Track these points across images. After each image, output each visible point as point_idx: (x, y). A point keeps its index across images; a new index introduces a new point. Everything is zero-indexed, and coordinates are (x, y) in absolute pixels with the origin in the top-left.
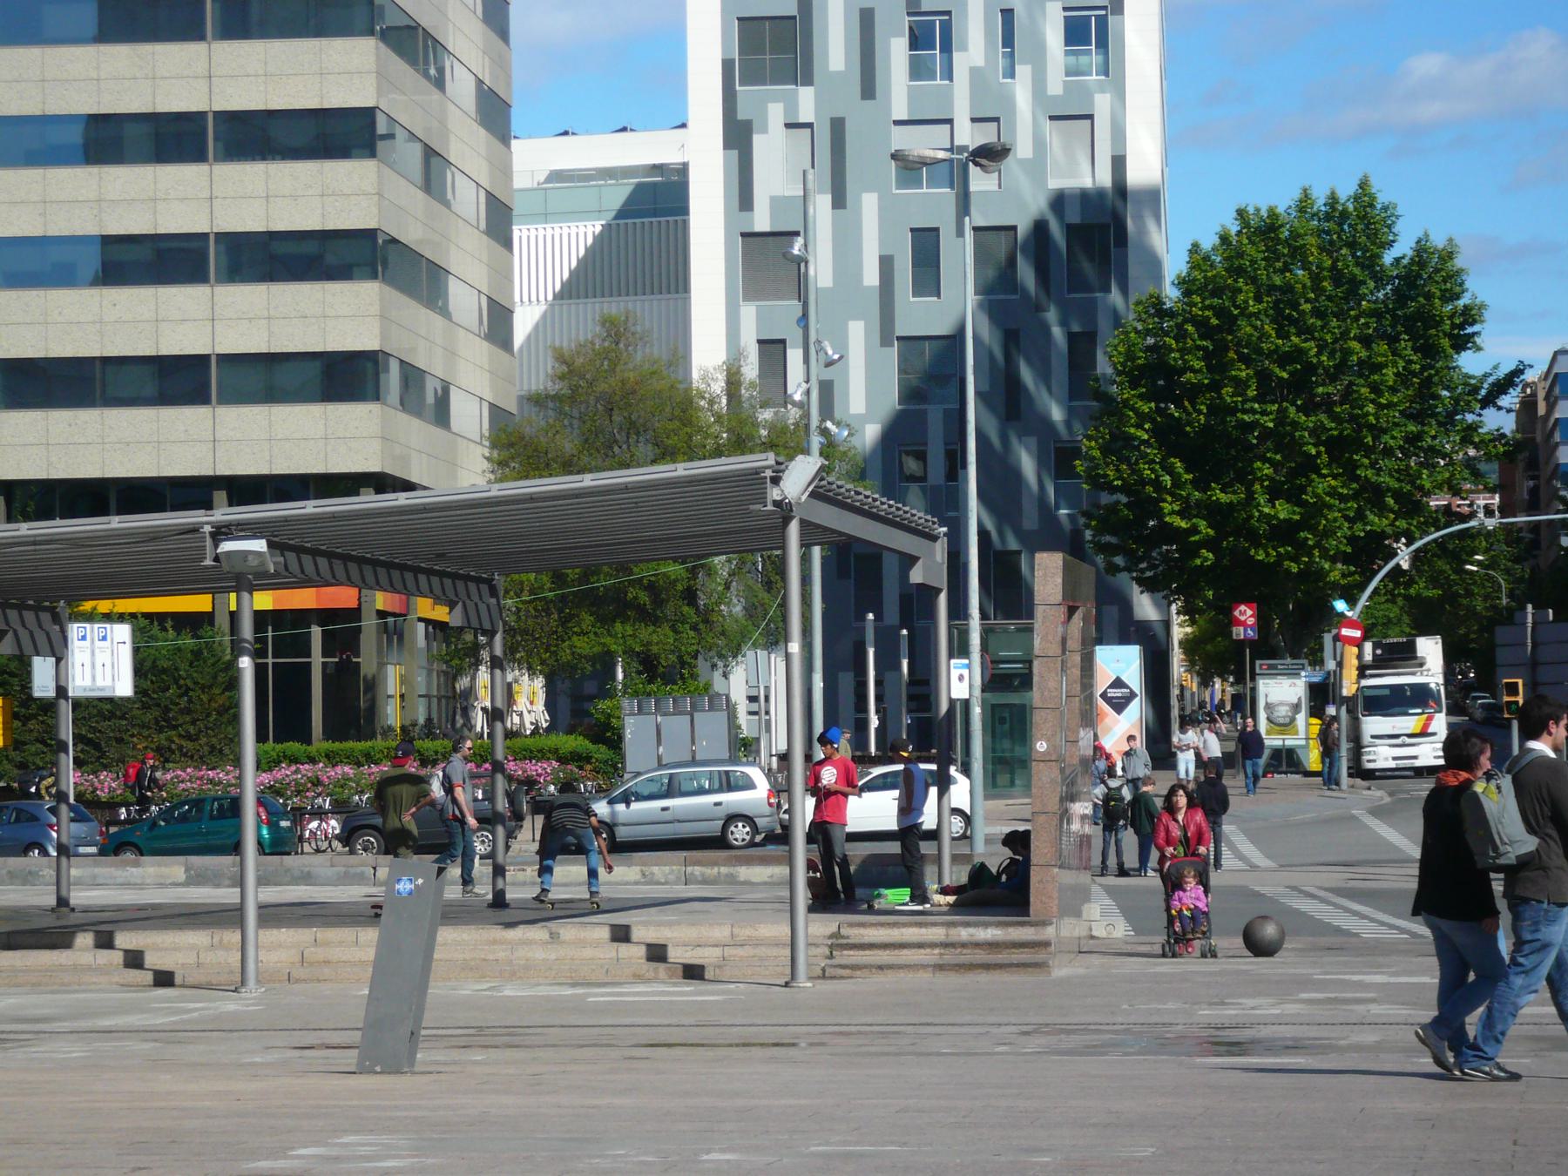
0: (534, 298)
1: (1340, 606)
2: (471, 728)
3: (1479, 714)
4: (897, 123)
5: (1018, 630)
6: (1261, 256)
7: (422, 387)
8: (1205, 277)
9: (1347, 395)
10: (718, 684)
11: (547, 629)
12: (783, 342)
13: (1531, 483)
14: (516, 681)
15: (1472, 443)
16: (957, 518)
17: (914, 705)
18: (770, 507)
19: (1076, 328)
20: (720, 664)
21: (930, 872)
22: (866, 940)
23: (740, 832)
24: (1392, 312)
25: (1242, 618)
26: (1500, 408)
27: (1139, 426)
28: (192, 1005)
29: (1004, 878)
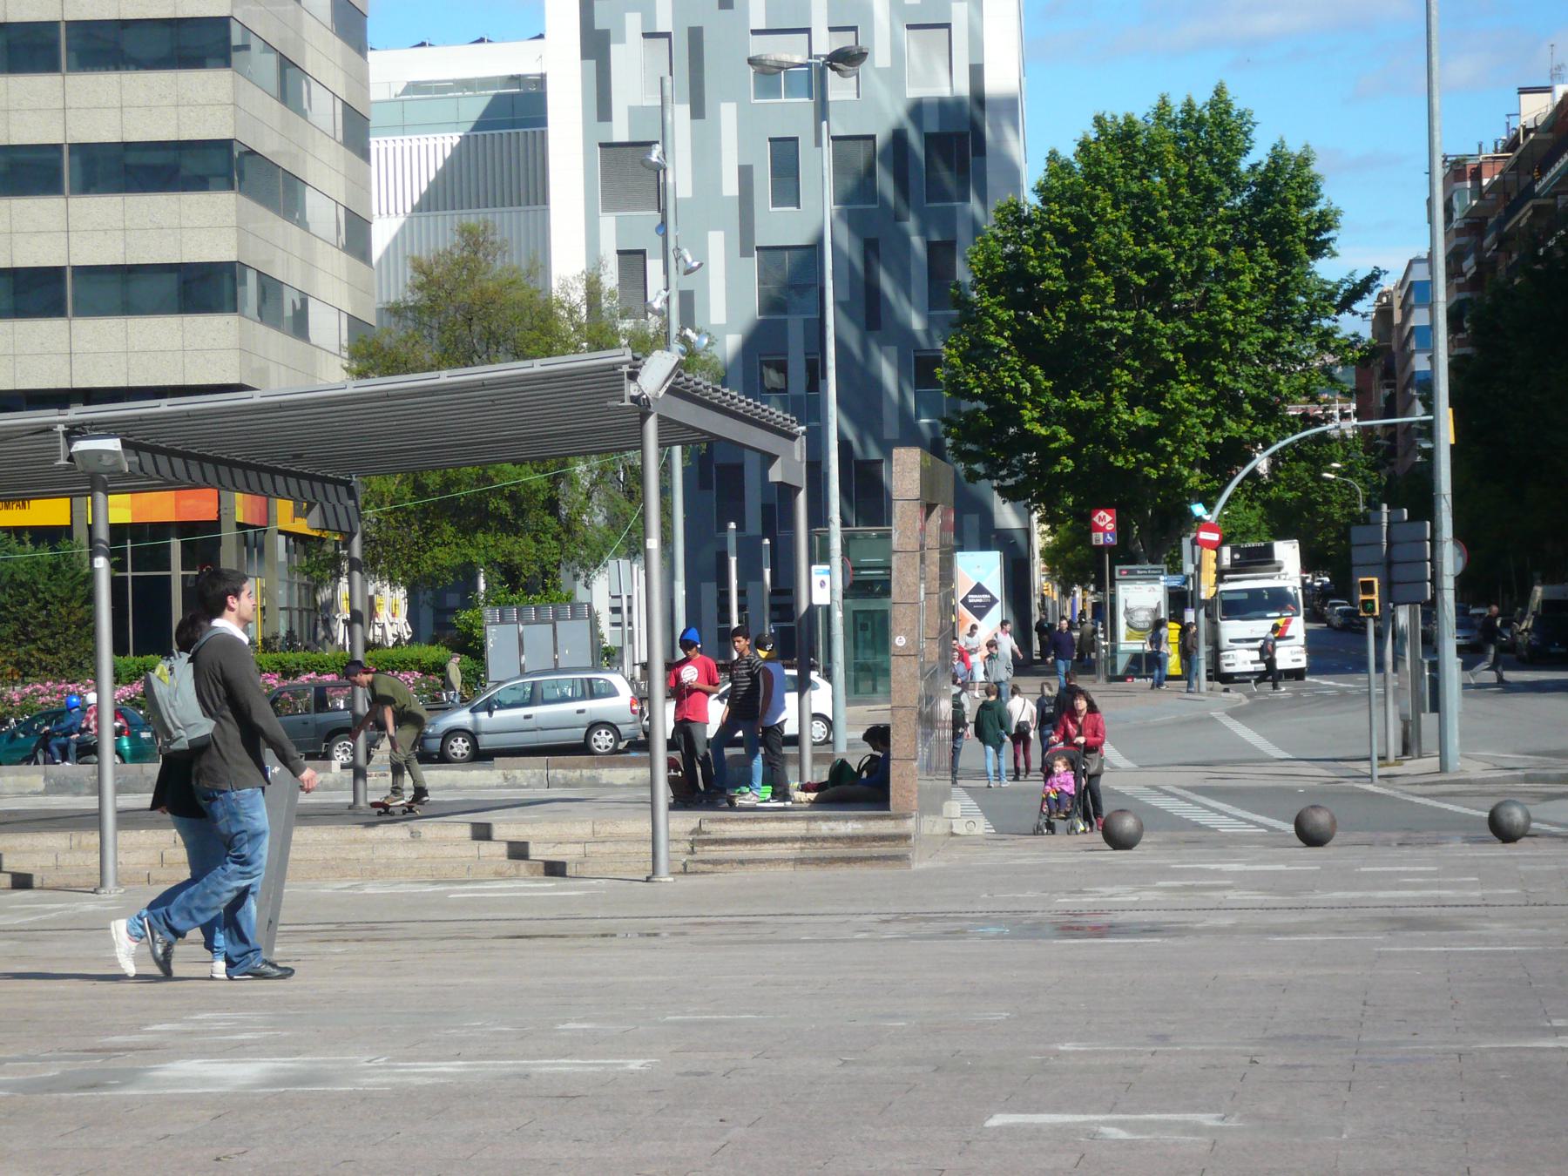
0: (392, 210)
1: (1198, 509)
2: (333, 640)
3: (1337, 621)
4: (754, 32)
5: (879, 536)
6: (1118, 163)
7: (280, 299)
8: (1063, 185)
9: (1204, 302)
10: (581, 594)
11: (408, 540)
12: (643, 252)
13: (1387, 391)
14: (377, 592)
15: (1328, 348)
16: (819, 428)
17: (777, 615)
18: (627, 403)
19: (936, 237)
20: (583, 574)
21: (791, 771)
22: (727, 835)
23: (603, 740)
24: (1249, 218)
25: (1102, 524)
26: (1355, 313)
27: (999, 334)
28: (50, 906)
29: (865, 775)
